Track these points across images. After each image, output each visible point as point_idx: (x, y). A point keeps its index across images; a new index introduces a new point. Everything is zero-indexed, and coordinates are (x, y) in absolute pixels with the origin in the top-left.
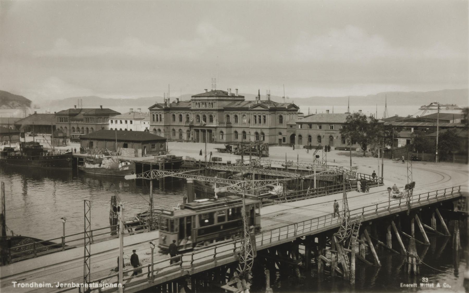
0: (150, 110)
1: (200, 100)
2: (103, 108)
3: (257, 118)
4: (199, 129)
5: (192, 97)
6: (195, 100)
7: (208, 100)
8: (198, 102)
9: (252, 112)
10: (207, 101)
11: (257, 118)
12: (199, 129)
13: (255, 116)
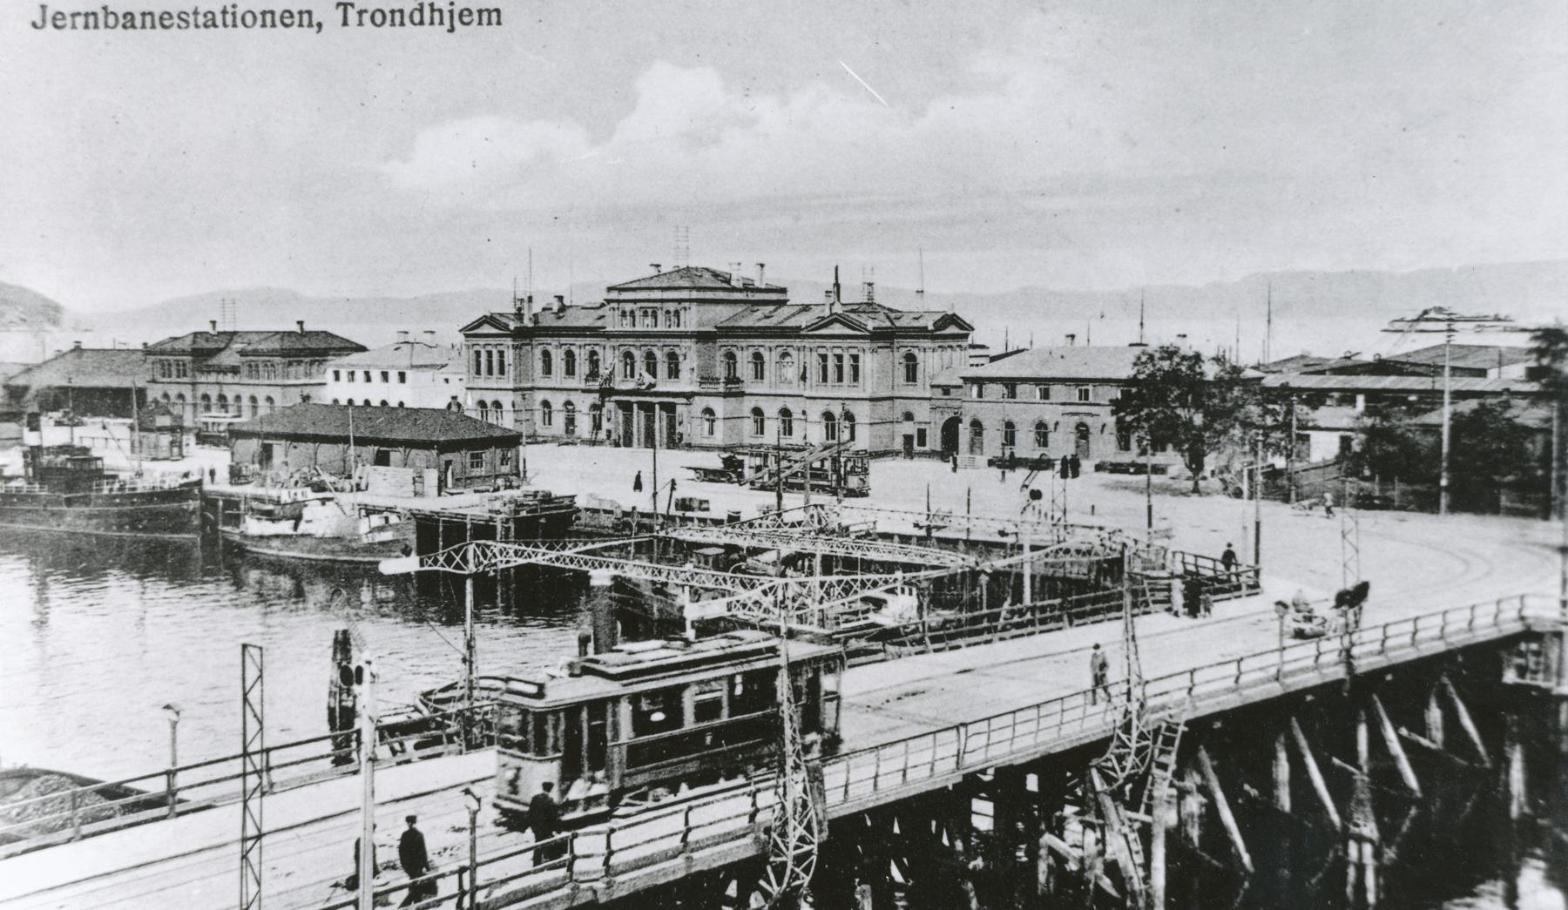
0: (467, 336)
1: (635, 301)
2: (308, 327)
4: (634, 399)
5: (610, 289)
6: (618, 301)
8: (628, 307)
9: (807, 343)
11: (483, 359)
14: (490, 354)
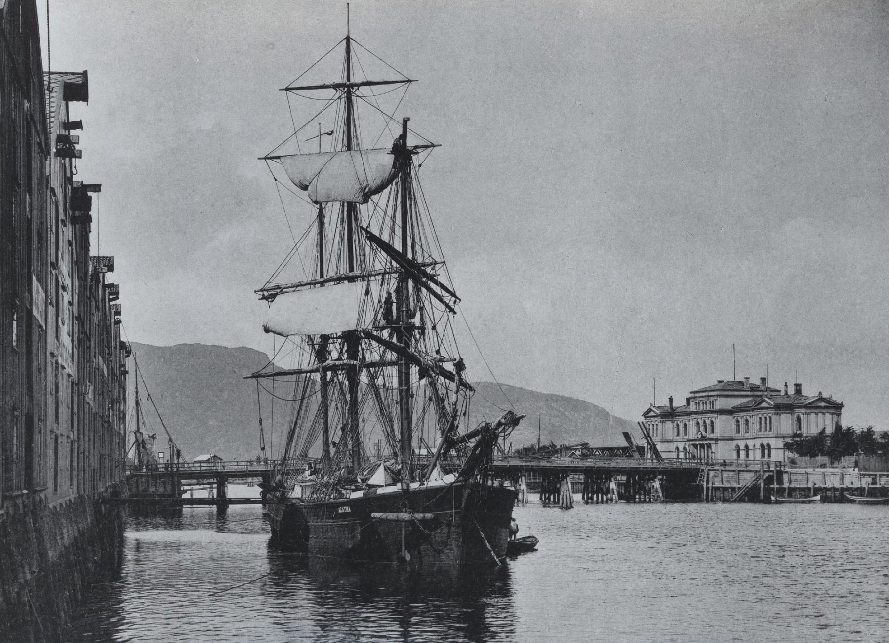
3: (763, 420)
7: (708, 396)
11: (763, 420)
13: (760, 418)
14: (765, 418)
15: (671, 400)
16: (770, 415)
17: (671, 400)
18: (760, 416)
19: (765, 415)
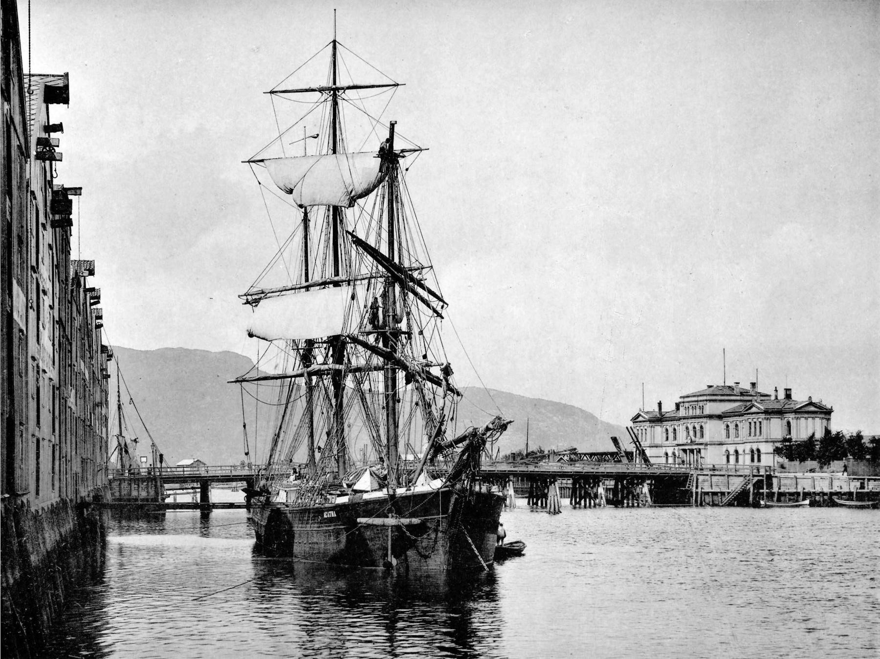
3: (753, 424)
7: (697, 401)
10: (696, 403)
11: (753, 424)
12: (686, 447)
13: (750, 423)
15: (660, 404)
16: (760, 420)
17: (660, 404)
18: (750, 420)
19: (755, 420)
